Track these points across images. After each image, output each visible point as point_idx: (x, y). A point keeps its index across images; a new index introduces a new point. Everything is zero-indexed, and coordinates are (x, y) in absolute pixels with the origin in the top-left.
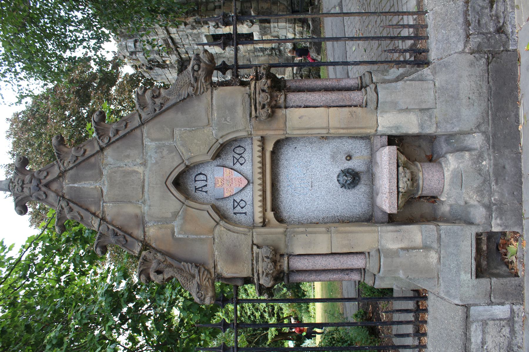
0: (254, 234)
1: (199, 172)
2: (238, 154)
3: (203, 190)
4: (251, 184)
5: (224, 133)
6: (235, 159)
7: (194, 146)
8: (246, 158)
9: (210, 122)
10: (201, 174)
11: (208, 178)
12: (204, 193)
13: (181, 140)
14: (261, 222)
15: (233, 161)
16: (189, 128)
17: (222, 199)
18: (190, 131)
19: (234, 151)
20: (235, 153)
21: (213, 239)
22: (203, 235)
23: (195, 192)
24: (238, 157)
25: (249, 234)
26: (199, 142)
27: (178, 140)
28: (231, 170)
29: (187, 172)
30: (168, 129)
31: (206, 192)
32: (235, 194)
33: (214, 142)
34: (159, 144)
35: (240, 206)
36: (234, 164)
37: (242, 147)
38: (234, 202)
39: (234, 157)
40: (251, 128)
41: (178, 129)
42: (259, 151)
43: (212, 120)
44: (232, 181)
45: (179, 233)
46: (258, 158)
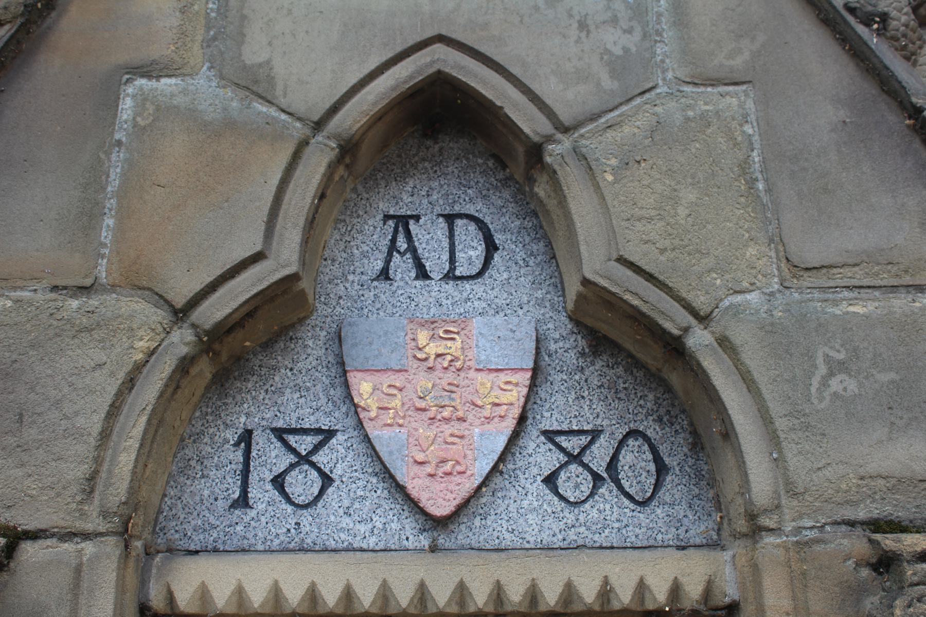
0: (89, 548)
1: (498, 238)
2: (614, 458)
3: (396, 258)
4: (424, 541)
5: (752, 359)
6: (584, 440)
7: (659, 187)
8: (590, 512)
9: (809, 280)
10: (491, 247)
11: (467, 286)
12: (379, 265)
13: (688, 119)
14: (171, 598)
15: (571, 432)
16: (764, 161)
17: (343, 364)
18: (744, 166)
19: (633, 433)
20: (622, 443)
21: (88, 282)
22: (120, 231)
23: (387, 217)
24: (599, 456)
25: (92, 509)
26: (682, 212)
27: (689, 106)
28: (516, 412)
29: (501, 176)
30: (747, 55)
31: (384, 275)
32: (367, 439)
33: (689, 297)
34: (659, 15)
35: (292, 466)
36: (550, 435)
37: (657, 486)
38: (319, 431)
39: (595, 434)
40: (798, 530)
41: (750, 105)
42: (641, 587)
43: (822, 289)
44: (447, 420)
45: (142, 100)
46: (596, 584)
